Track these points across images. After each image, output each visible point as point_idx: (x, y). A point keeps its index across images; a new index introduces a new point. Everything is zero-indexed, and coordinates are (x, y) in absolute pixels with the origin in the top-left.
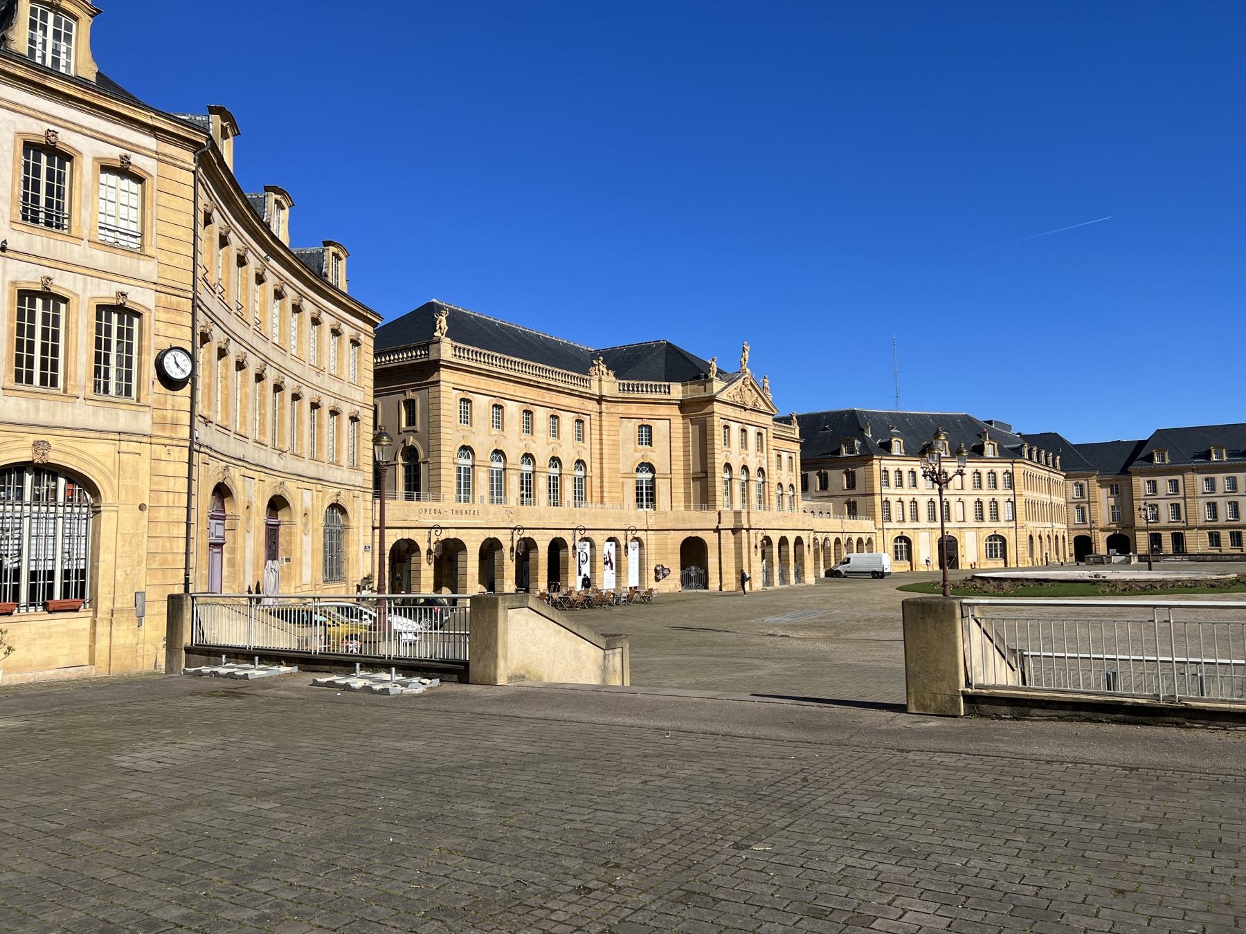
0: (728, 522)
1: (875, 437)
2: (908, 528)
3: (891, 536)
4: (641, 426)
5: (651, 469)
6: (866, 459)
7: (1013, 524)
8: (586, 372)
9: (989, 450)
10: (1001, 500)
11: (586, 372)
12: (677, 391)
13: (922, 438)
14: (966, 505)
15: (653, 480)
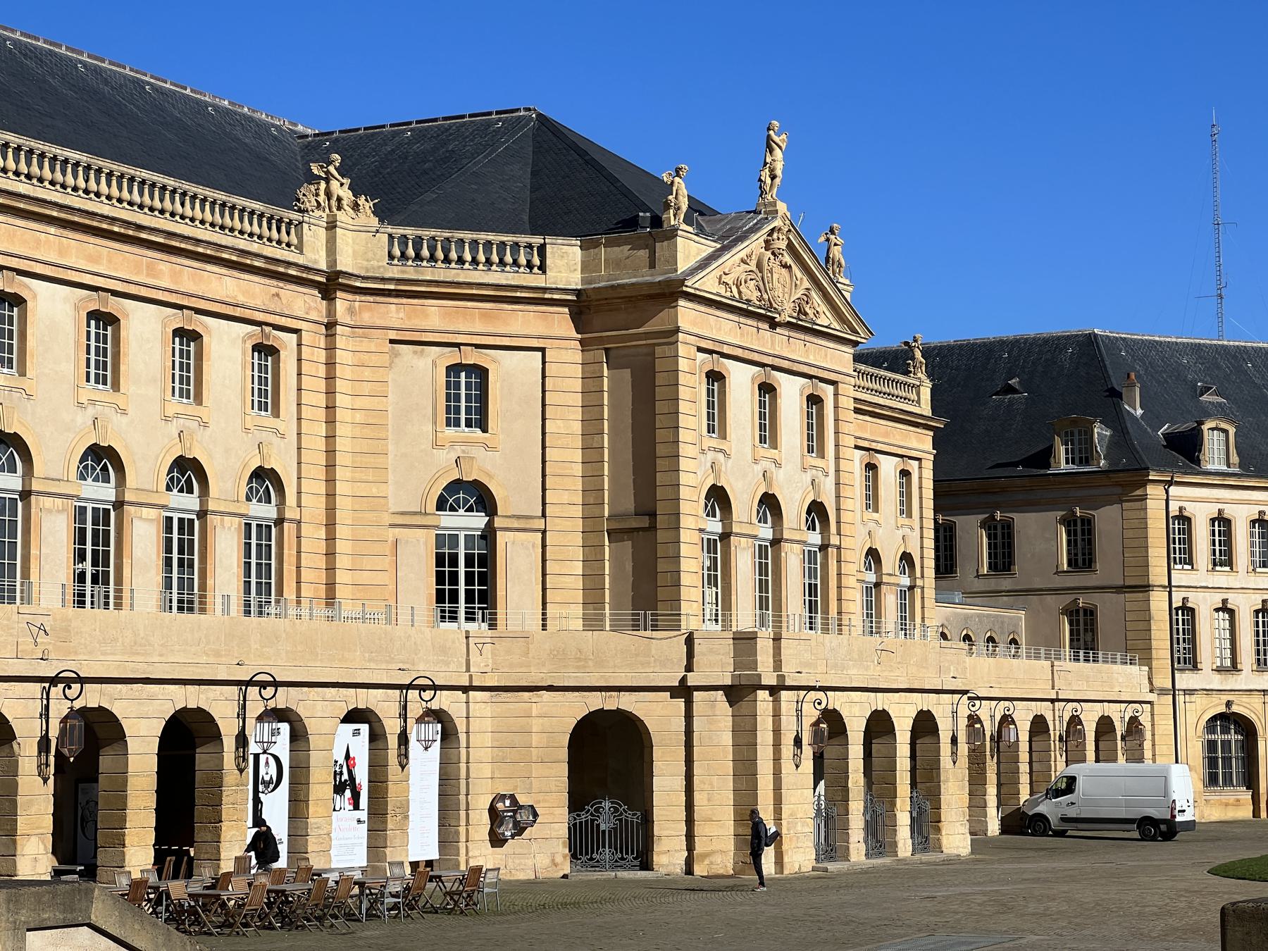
1: (1153, 417)
3: (1198, 711)
4: (453, 370)
6: (1127, 480)
11: (289, 200)
12: (566, 263)
15: (489, 535)
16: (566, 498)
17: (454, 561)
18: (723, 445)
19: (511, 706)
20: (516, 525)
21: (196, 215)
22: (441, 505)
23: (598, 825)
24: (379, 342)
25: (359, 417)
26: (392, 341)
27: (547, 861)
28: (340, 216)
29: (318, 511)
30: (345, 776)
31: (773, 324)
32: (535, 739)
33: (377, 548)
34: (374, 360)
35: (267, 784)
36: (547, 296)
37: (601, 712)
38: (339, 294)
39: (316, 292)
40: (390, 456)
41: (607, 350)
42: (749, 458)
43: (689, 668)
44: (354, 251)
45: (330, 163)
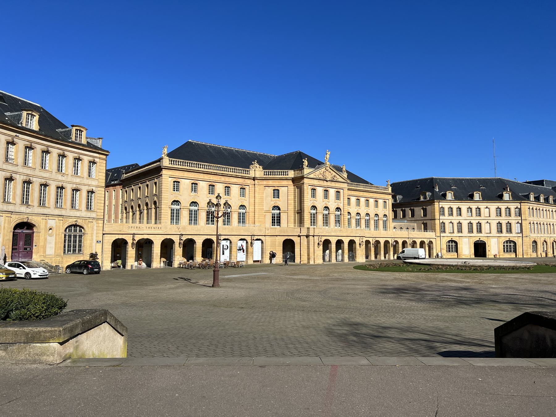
0: (304, 232)
1: (440, 191)
2: (456, 236)
3: (445, 241)
4: (274, 190)
5: (279, 209)
6: (431, 202)
7: (521, 235)
9: (506, 196)
10: (513, 223)
12: (291, 174)
13: (465, 190)
14: (492, 225)
15: (280, 213)
21: (230, 170)
24: (262, 187)
31: (327, 181)
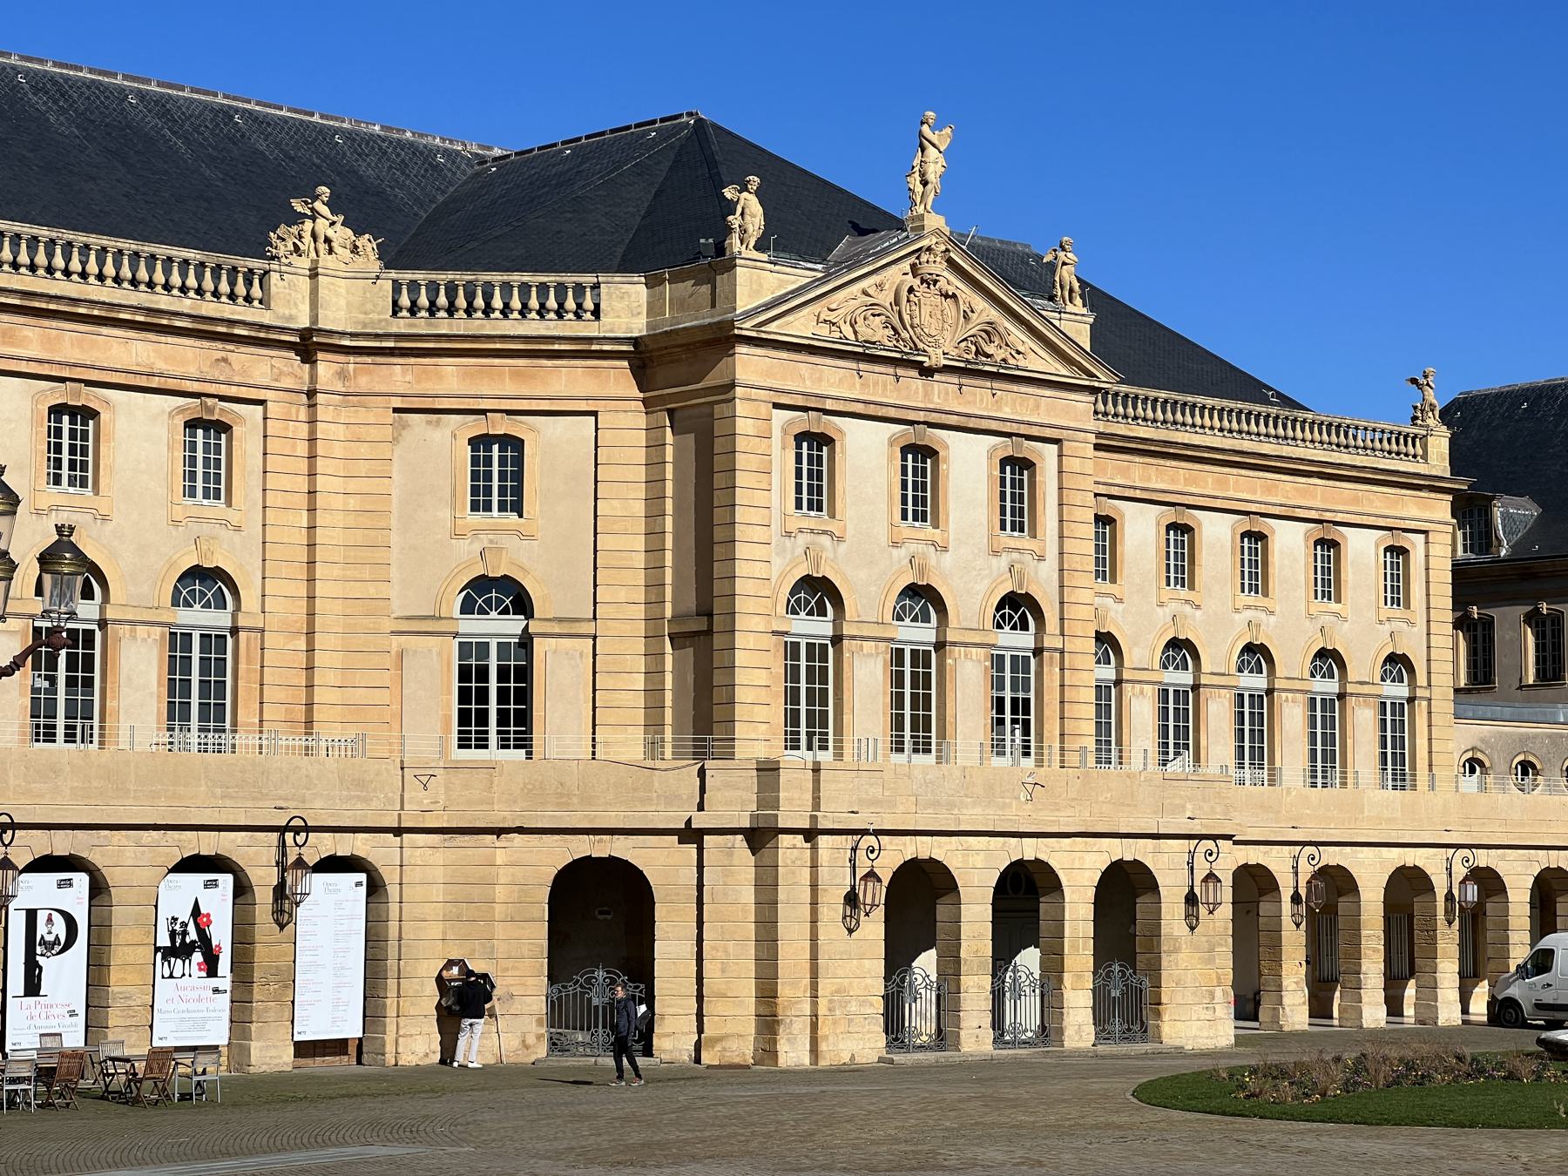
0: (733, 801)
5: (522, 604)
8: (259, 249)
11: (259, 249)
12: (627, 306)
15: (526, 642)
16: (622, 595)
17: (483, 674)
18: (832, 526)
19: (469, 852)
20: (557, 630)
22: (467, 607)
23: (590, 1000)
25: (353, 503)
26: (396, 410)
27: (516, 1043)
28: (326, 261)
29: (295, 617)
30: (193, 935)
31: (927, 372)
32: (500, 893)
33: (376, 660)
34: (374, 433)
35: (49, 946)
36: (594, 347)
37: (588, 859)
38: (320, 355)
39: (292, 354)
40: (395, 550)
41: (671, 412)
42: (884, 540)
43: (816, 805)
44: (348, 304)
45: (316, 198)
